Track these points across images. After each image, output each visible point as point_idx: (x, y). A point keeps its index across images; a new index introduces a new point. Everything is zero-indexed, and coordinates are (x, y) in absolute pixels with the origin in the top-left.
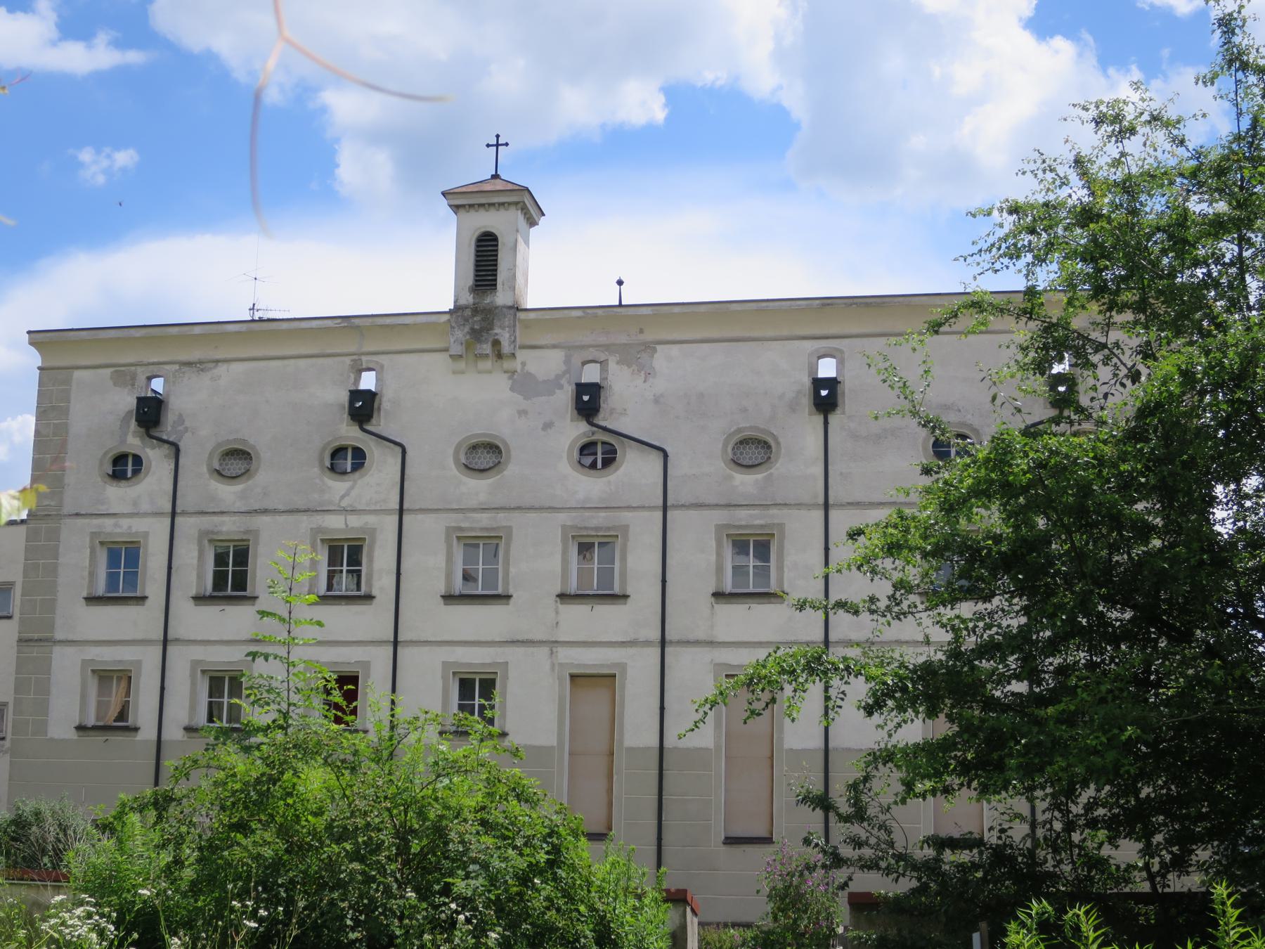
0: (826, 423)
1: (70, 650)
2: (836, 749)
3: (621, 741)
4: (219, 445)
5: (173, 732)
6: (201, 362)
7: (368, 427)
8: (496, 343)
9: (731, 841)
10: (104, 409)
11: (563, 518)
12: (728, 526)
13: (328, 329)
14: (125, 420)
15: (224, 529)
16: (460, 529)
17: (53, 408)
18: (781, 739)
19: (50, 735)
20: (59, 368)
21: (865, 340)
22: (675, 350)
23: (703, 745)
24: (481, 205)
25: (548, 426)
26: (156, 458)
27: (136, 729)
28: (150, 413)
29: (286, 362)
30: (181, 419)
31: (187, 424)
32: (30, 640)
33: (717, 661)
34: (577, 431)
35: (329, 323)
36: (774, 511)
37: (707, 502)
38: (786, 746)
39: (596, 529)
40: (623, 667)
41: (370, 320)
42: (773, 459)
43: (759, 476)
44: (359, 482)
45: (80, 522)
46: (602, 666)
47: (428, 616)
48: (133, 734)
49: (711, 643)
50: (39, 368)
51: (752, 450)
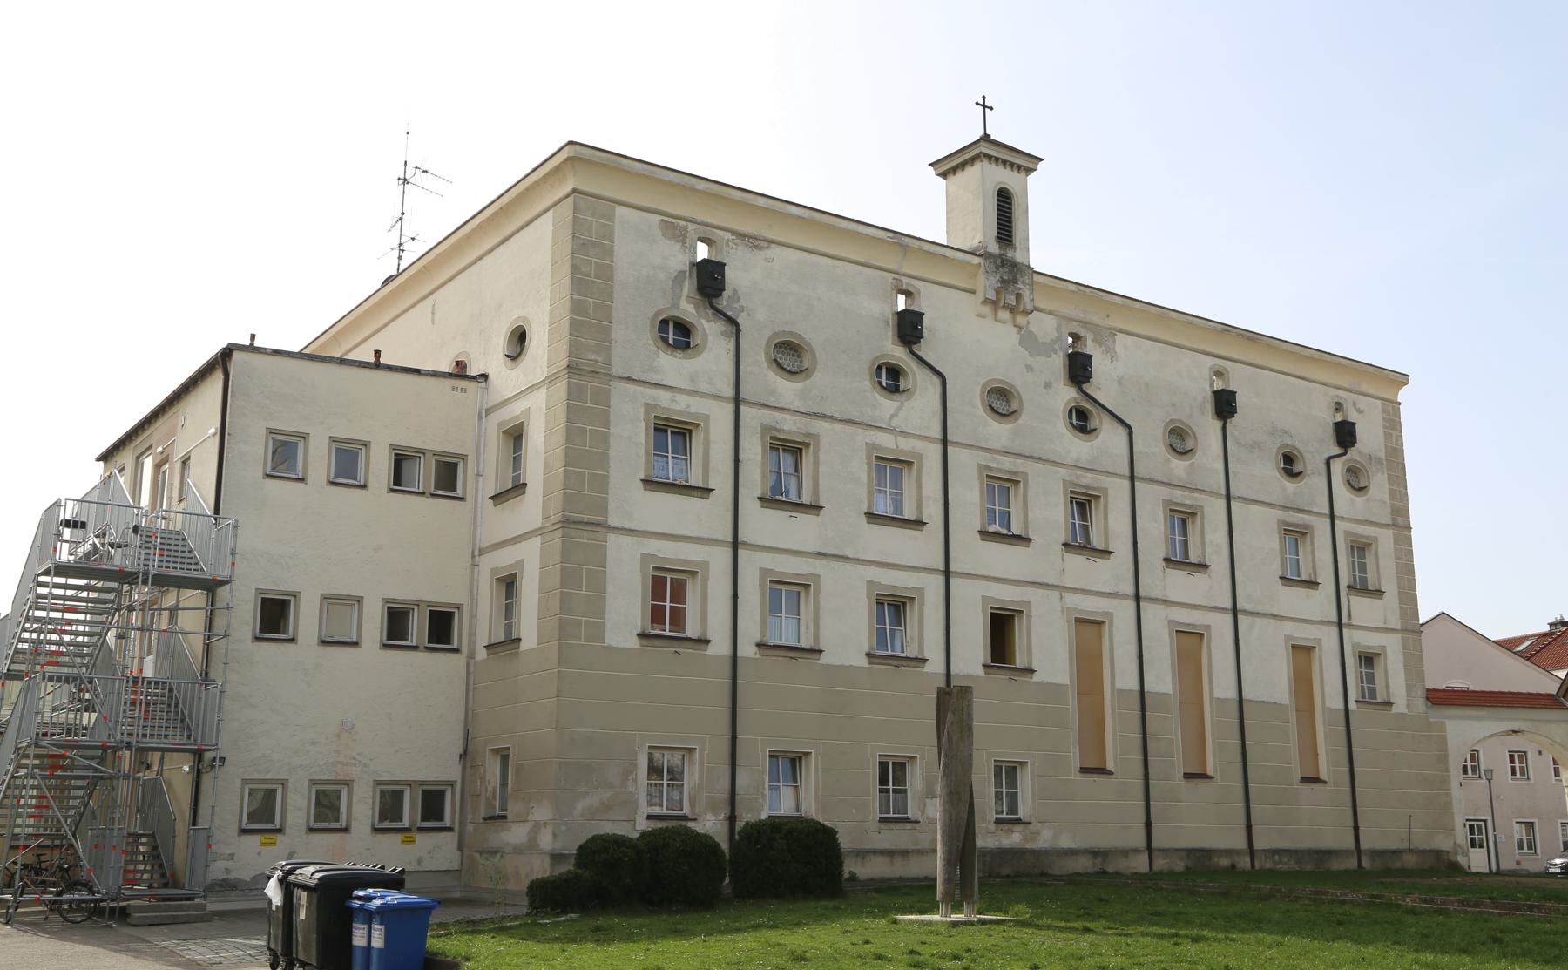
0: (1224, 429)
1: (626, 540)
4: (776, 334)
5: (747, 650)
6: (755, 238)
8: (1019, 296)
9: (1188, 776)
10: (650, 263)
12: (1071, 483)
13: (874, 238)
14: (679, 278)
16: (990, 468)
17: (595, 244)
19: (608, 642)
20: (593, 196)
24: (1004, 162)
26: (709, 329)
28: (709, 279)
29: (835, 262)
30: (735, 296)
31: (743, 302)
32: (580, 522)
34: (1067, 395)
35: (1072, 287)
39: (1087, 487)
40: (1110, 615)
45: (631, 387)
47: (972, 553)
49: (1165, 602)
51: (1179, 440)
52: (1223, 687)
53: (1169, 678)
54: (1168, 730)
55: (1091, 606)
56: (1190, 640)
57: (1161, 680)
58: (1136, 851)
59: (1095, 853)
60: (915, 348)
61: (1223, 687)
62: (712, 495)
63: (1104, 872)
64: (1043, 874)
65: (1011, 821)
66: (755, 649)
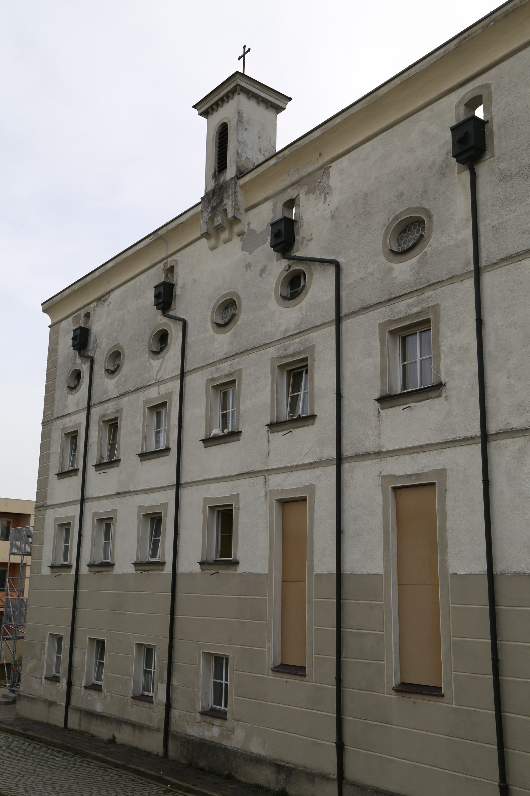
2: (502, 574)
3: (311, 568)
7: (171, 313)
11: (272, 352)
15: (109, 412)
16: (213, 379)
18: (445, 561)
21: (513, 59)
22: (344, 161)
23: (375, 571)
25: (263, 271)
27: (236, 563)
29: (136, 279)
33: (385, 473)
34: (279, 267)
35: (148, 241)
36: (429, 294)
37: (372, 303)
38: (451, 571)
39: (293, 355)
41: (165, 228)
42: (426, 235)
43: (415, 260)
44: (166, 357)
46: (297, 489)
48: (110, 569)
50: (49, 327)
52: (323, 563)
53: (379, 553)
54: (378, 627)
55: (290, 483)
56: (414, 501)
57: (369, 555)
58: (325, 777)
59: (280, 768)
60: (171, 313)
61: (323, 563)
62: (242, 437)
63: (113, 741)
64: (230, 778)
65: (214, 714)
66: (87, 568)
